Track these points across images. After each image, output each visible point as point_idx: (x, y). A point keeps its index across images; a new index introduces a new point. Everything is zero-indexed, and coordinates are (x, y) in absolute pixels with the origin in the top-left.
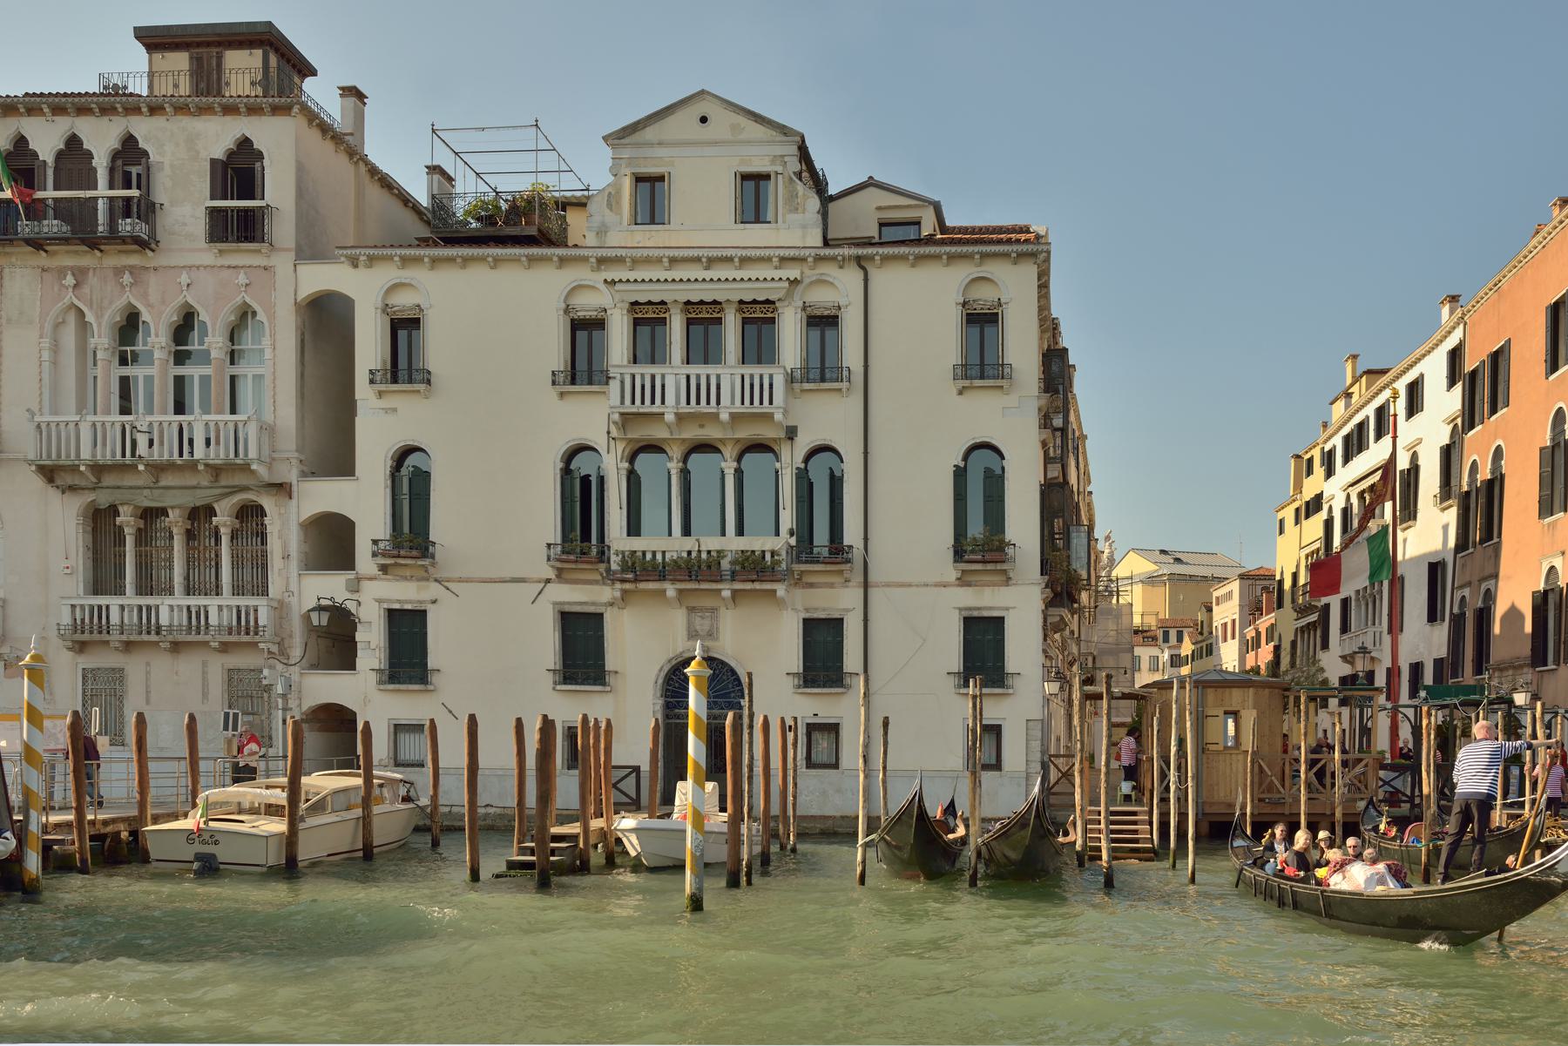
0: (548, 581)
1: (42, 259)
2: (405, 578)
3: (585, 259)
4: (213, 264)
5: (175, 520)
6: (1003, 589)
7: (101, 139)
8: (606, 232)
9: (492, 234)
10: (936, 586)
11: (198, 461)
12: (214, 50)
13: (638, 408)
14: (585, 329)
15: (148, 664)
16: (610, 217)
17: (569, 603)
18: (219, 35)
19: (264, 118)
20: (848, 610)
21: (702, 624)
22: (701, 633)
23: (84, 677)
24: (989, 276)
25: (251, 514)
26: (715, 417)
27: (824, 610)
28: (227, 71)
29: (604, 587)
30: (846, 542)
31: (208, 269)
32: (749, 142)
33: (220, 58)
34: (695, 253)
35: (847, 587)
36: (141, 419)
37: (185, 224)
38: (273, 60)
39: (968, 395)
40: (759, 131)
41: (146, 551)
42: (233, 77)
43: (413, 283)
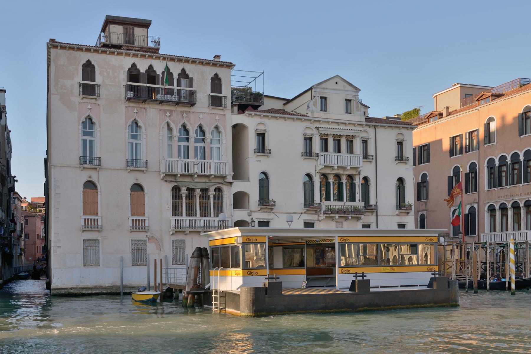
0: (302, 213)
1: (160, 107)
2: (265, 212)
3: (310, 120)
4: (209, 112)
5: (198, 193)
7: (176, 69)
9: (251, 104)
10: (392, 216)
12: (131, 27)
14: (309, 140)
15: (192, 238)
16: (314, 108)
17: (307, 220)
18: (135, 22)
20: (372, 222)
23: (173, 242)
25: (218, 190)
28: (135, 35)
29: (316, 215)
30: (406, 202)
31: (209, 114)
32: (348, 91)
33: (133, 29)
34: (337, 121)
36: (191, 159)
37: (200, 99)
39: (398, 164)
40: (349, 88)
42: (137, 37)
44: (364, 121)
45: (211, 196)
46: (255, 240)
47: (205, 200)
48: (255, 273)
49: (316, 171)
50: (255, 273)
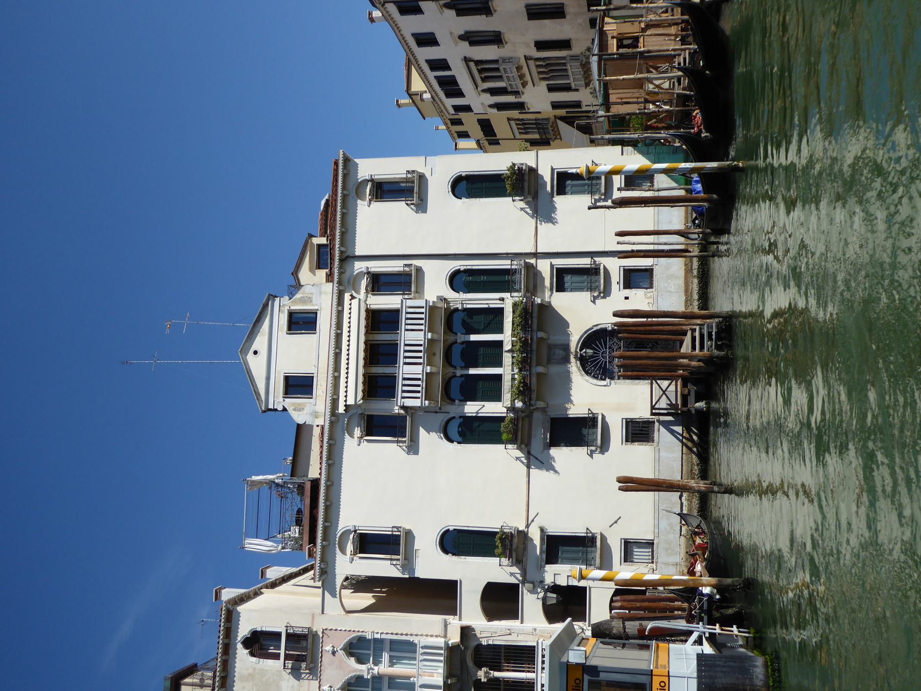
8: (316, 412)
11: (444, 683)
38: (187, 680)
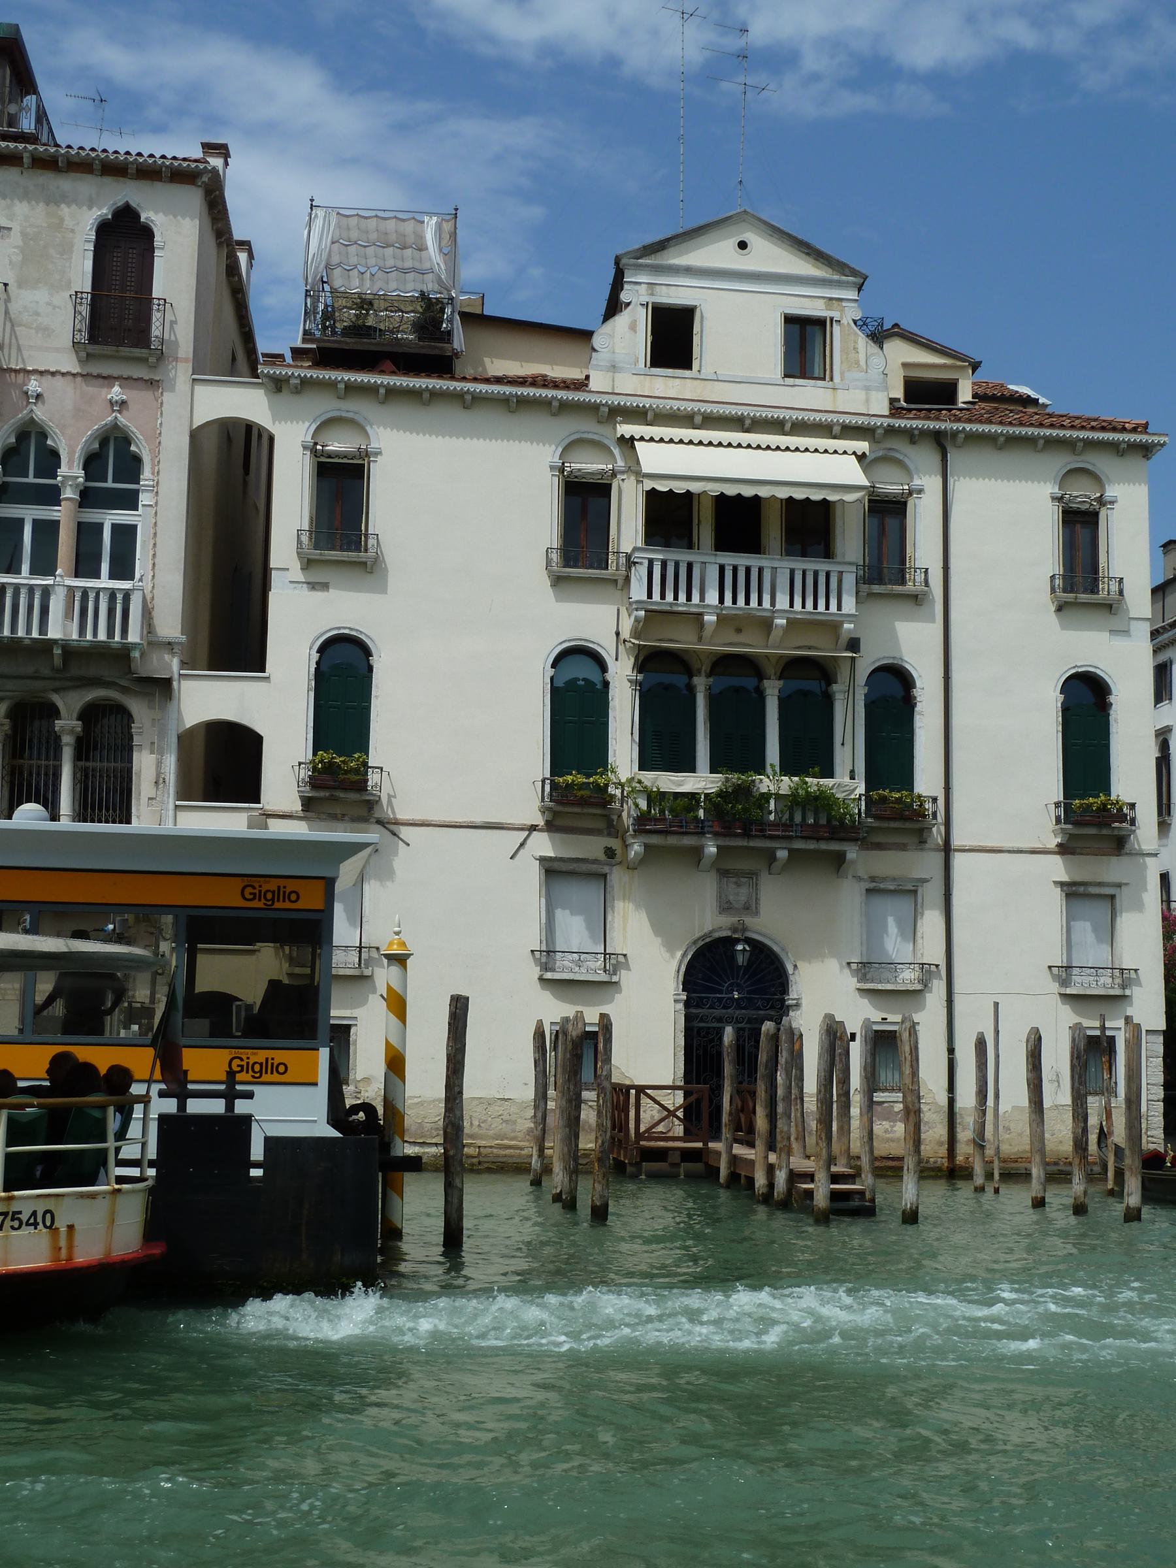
6: (1114, 859)
11: (54, 642)
13: (671, 604)
19: (158, 185)
21: (739, 894)
22: (735, 905)
24: (1090, 467)
26: (766, 624)
27: (894, 879)
35: (922, 850)
37: (37, 314)
41: (47, 767)
43: (356, 417)
44: (887, 413)
45: (67, 740)
46: (287, 897)
47: (47, 767)
48: (275, 1069)
49: (618, 634)
50: (275, 1069)
